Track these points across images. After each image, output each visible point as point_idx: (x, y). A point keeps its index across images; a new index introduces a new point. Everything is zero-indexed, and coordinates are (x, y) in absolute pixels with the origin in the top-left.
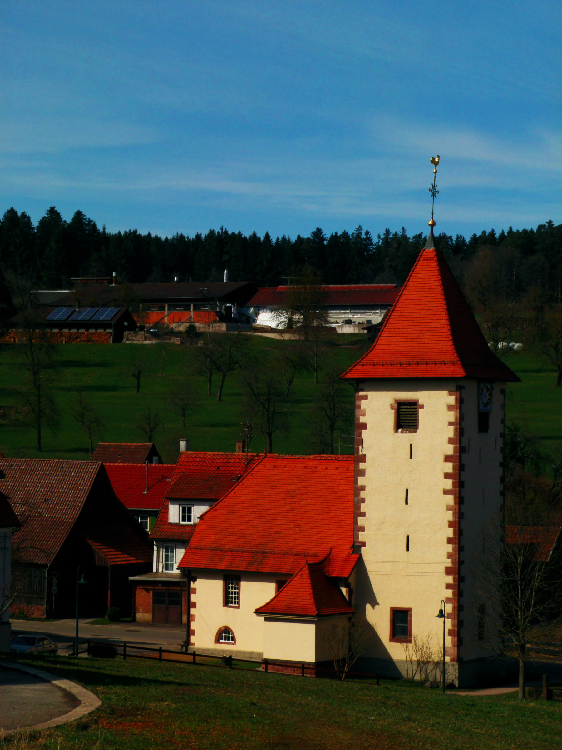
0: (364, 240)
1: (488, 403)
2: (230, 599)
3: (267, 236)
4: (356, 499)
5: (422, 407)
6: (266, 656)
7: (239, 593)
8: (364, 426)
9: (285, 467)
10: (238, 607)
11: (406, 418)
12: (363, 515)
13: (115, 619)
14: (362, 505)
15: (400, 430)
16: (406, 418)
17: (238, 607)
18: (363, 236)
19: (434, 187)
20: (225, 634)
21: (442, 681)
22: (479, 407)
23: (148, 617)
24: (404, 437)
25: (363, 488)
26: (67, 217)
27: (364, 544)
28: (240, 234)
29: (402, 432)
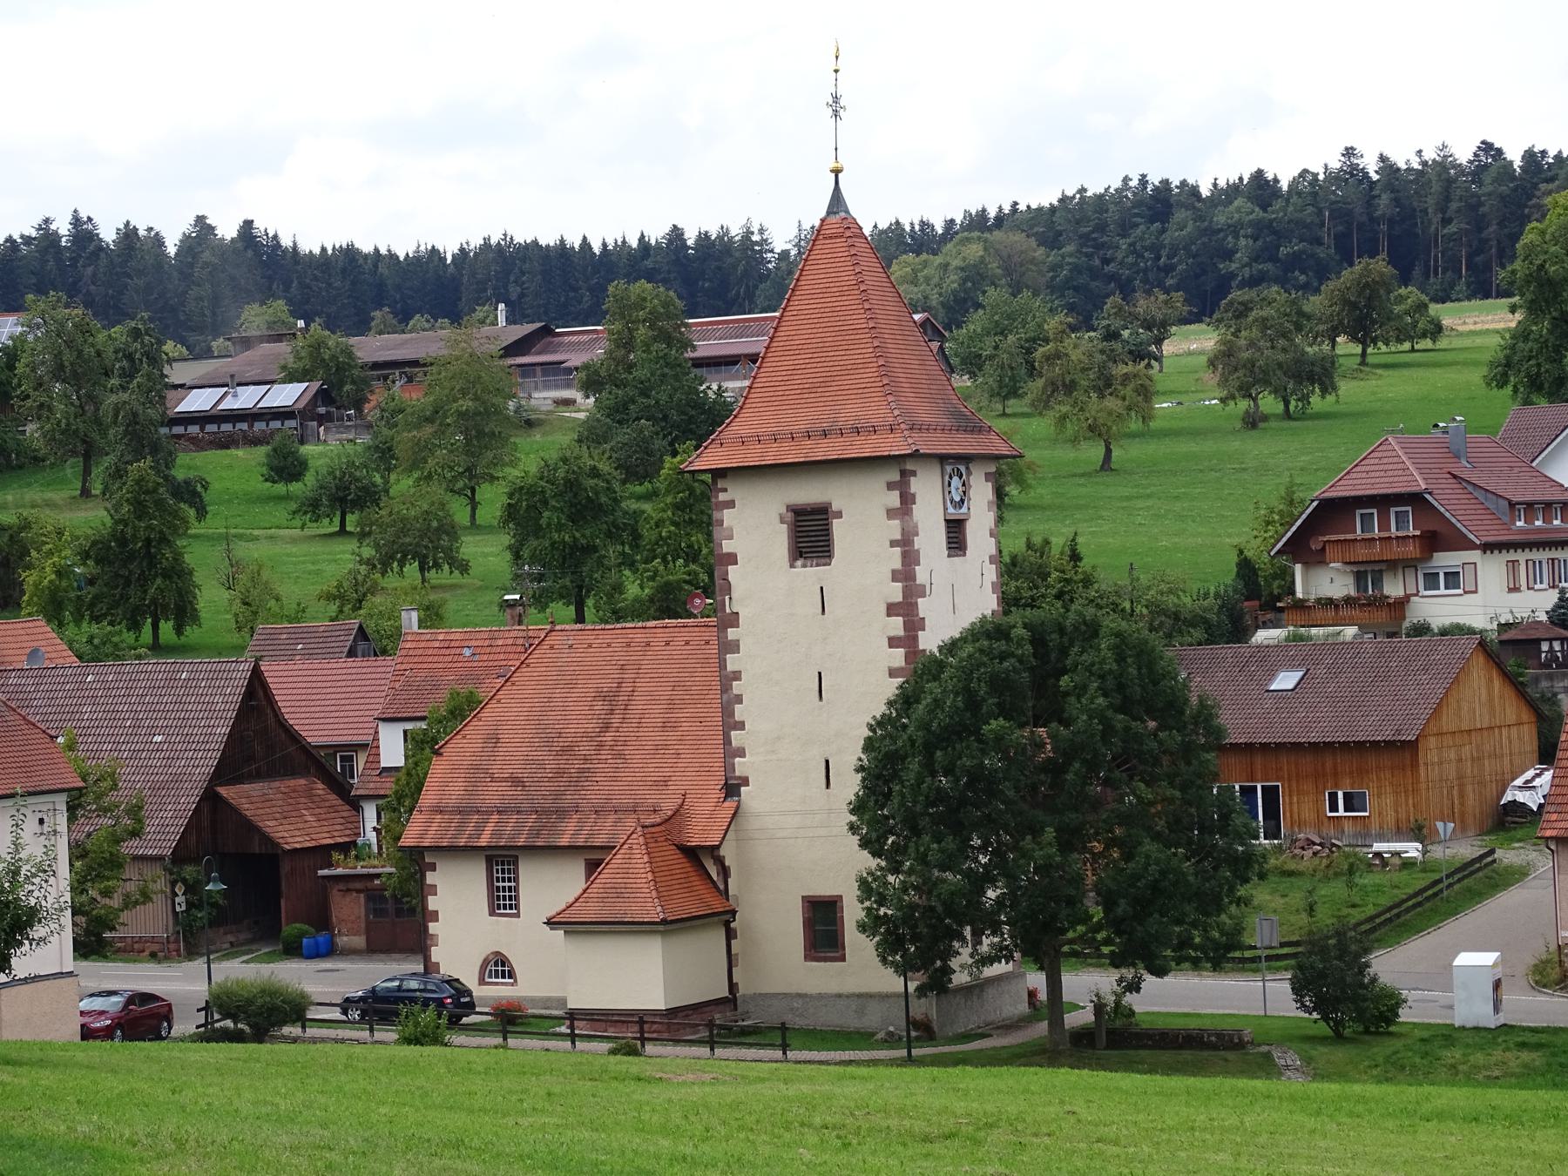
0: (756, 243)
1: (962, 501)
2: (503, 901)
3: (585, 243)
4: (725, 697)
5: (839, 515)
6: (572, 1004)
7: (516, 889)
8: (732, 559)
9: (590, 646)
10: (518, 915)
11: (811, 536)
12: (741, 726)
13: (293, 950)
14: (737, 707)
15: (799, 563)
16: (811, 536)
17: (518, 915)
18: (756, 238)
19: (836, 99)
20: (499, 966)
21: (1292, 962)
22: (945, 509)
23: (359, 941)
24: (809, 575)
25: (737, 676)
26: (227, 230)
27: (745, 781)
28: (535, 242)
29: (804, 566)
